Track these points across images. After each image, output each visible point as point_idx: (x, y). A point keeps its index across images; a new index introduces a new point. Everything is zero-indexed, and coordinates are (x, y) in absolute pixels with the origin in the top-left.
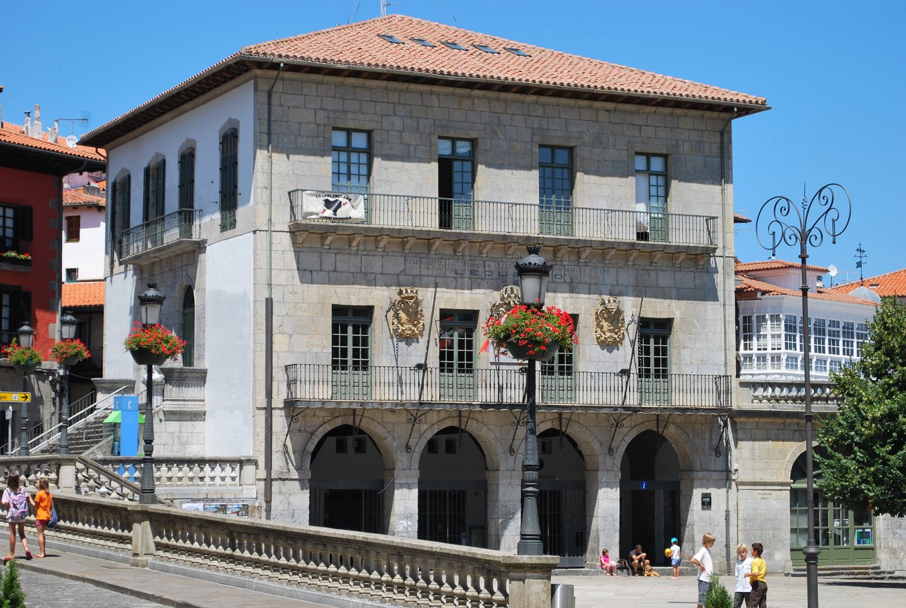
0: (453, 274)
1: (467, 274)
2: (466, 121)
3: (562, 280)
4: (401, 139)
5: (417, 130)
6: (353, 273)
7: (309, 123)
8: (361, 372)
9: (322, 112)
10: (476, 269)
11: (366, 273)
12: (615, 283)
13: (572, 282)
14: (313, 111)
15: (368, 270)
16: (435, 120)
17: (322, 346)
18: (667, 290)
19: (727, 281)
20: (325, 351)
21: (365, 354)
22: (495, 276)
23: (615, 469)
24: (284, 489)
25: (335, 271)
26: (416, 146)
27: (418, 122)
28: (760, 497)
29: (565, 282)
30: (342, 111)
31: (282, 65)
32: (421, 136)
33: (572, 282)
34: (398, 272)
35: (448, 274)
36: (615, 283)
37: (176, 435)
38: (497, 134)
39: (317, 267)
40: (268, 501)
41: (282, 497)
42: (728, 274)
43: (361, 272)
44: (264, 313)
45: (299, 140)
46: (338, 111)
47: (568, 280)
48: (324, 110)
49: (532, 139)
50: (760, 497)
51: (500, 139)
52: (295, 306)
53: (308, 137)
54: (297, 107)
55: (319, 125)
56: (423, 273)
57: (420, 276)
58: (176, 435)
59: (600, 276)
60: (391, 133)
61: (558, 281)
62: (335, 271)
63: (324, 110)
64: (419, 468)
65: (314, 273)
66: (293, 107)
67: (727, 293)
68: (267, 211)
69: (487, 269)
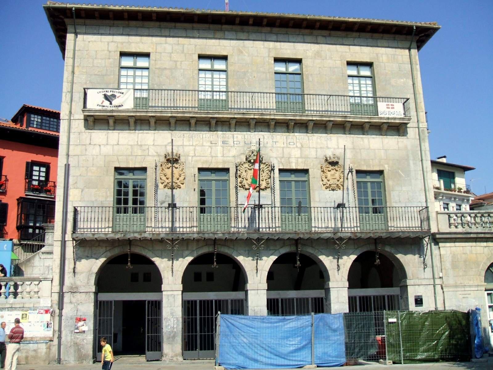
0: (209, 144)
1: (220, 143)
2: (219, 45)
3: (295, 146)
4: (170, 57)
5: (183, 52)
6: (131, 145)
7: (104, 51)
8: (139, 215)
9: (113, 43)
10: (226, 140)
11: (141, 145)
12: (336, 147)
13: (302, 146)
14: (106, 43)
15: (143, 144)
16: (196, 46)
17: (108, 196)
18: (377, 151)
19: (422, 144)
20: (108, 199)
21: (119, 193)
22: (242, 144)
23: (343, 279)
24: (74, 300)
25: (118, 144)
26: (181, 61)
27: (183, 47)
28: (461, 296)
29: (297, 147)
30: (128, 43)
31: (73, 9)
32: (185, 56)
33: (302, 146)
34: (165, 143)
35: (205, 144)
36: (336, 147)
37: (51, 268)
38: (242, 52)
39: (104, 142)
40: (61, 307)
41: (72, 306)
42: (424, 139)
43: (138, 145)
44: (63, 174)
45: (96, 61)
46: (124, 42)
47: (299, 145)
48: (114, 42)
49: (269, 55)
50: (461, 296)
51: (245, 55)
52: (87, 170)
53: (102, 59)
54: (95, 41)
55: (110, 52)
56: (185, 144)
57: (183, 146)
58: (51, 268)
59: (325, 143)
60: (163, 54)
61: (291, 146)
62: (118, 144)
63: (114, 42)
64: (182, 283)
65: (102, 147)
66: (92, 41)
67: (423, 152)
68: (68, 107)
69: (235, 140)
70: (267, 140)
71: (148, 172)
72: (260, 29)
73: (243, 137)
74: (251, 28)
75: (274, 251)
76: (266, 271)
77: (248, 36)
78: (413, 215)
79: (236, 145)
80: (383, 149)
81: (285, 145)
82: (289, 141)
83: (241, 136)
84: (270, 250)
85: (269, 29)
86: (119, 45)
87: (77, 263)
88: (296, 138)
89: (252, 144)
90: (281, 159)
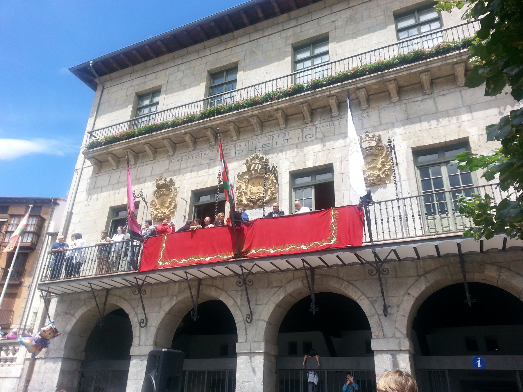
3: (314, 138)
23: (398, 335)
70: (276, 140)
71: (363, 181)
72: (275, 20)
73: (247, 144)
74: (265, 23)
75: (277, 289)
76: (264, 321)
77: (331, 10)
78: (391, 214)
79: (238, 155)
80: (463, 106)
81: (301, 140)
82: (305, 134)
83: (245, 143)
84: (272, 287)
85: (285, 16)
86: (137, 87)
87: (387, 337)
88: (316, 127)
89: (257, 150)
90: (293, 159)
